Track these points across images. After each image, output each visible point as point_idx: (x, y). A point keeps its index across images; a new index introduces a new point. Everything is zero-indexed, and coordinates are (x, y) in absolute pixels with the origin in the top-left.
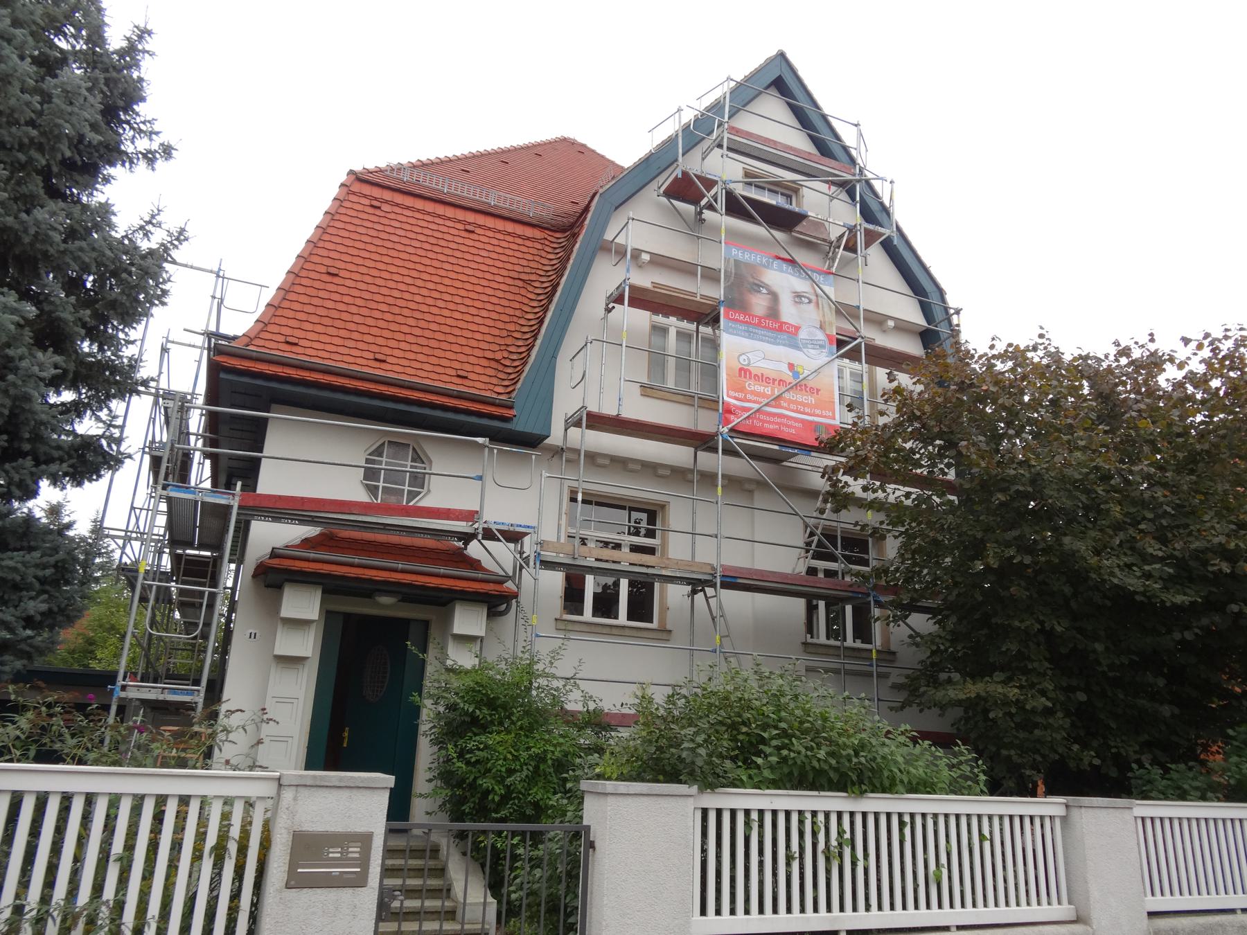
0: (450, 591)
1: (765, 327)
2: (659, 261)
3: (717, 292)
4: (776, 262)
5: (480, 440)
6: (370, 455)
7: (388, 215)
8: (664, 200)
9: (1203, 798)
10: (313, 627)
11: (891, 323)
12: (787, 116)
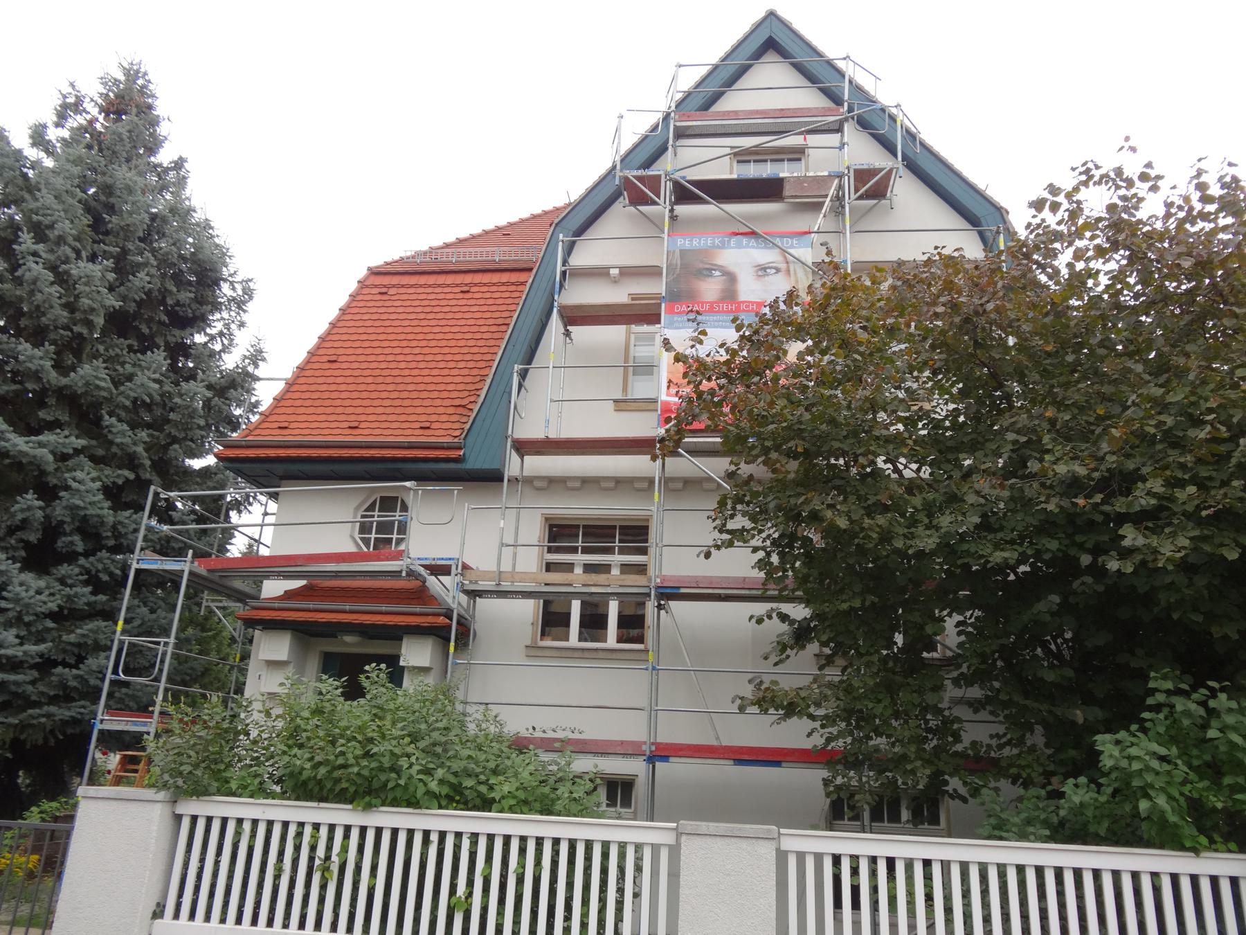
0: (396, 627)
1: (718, 312)
2: (628, 272)
3: (659, 287)
4: (734, 240)
5: (408, 484)
6: (366, 511)
7: (393, 298)
8: (632, 208)
9: (1023, 836)
10: (292, 665)
11: (614, 272)
12: (794, 78)
